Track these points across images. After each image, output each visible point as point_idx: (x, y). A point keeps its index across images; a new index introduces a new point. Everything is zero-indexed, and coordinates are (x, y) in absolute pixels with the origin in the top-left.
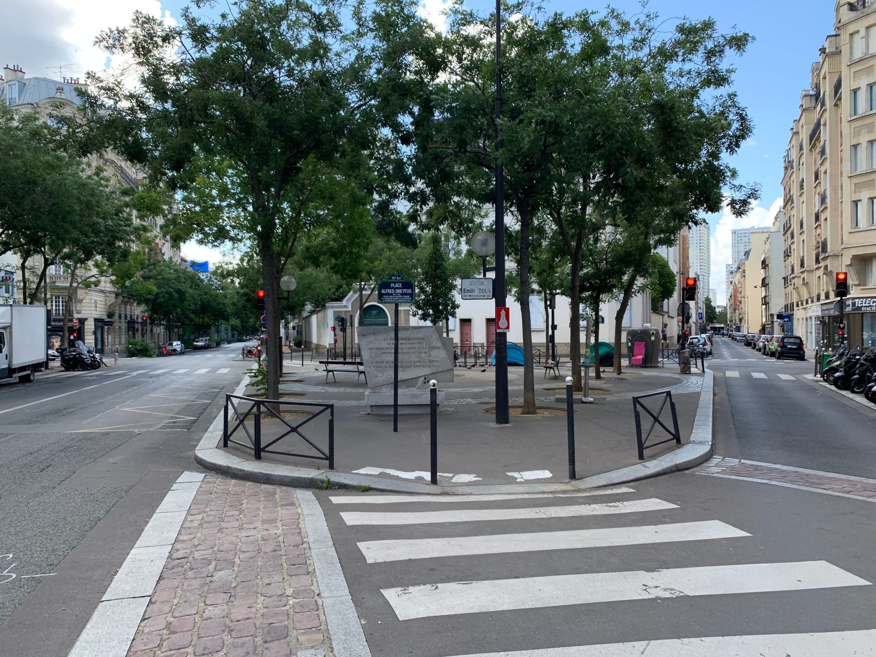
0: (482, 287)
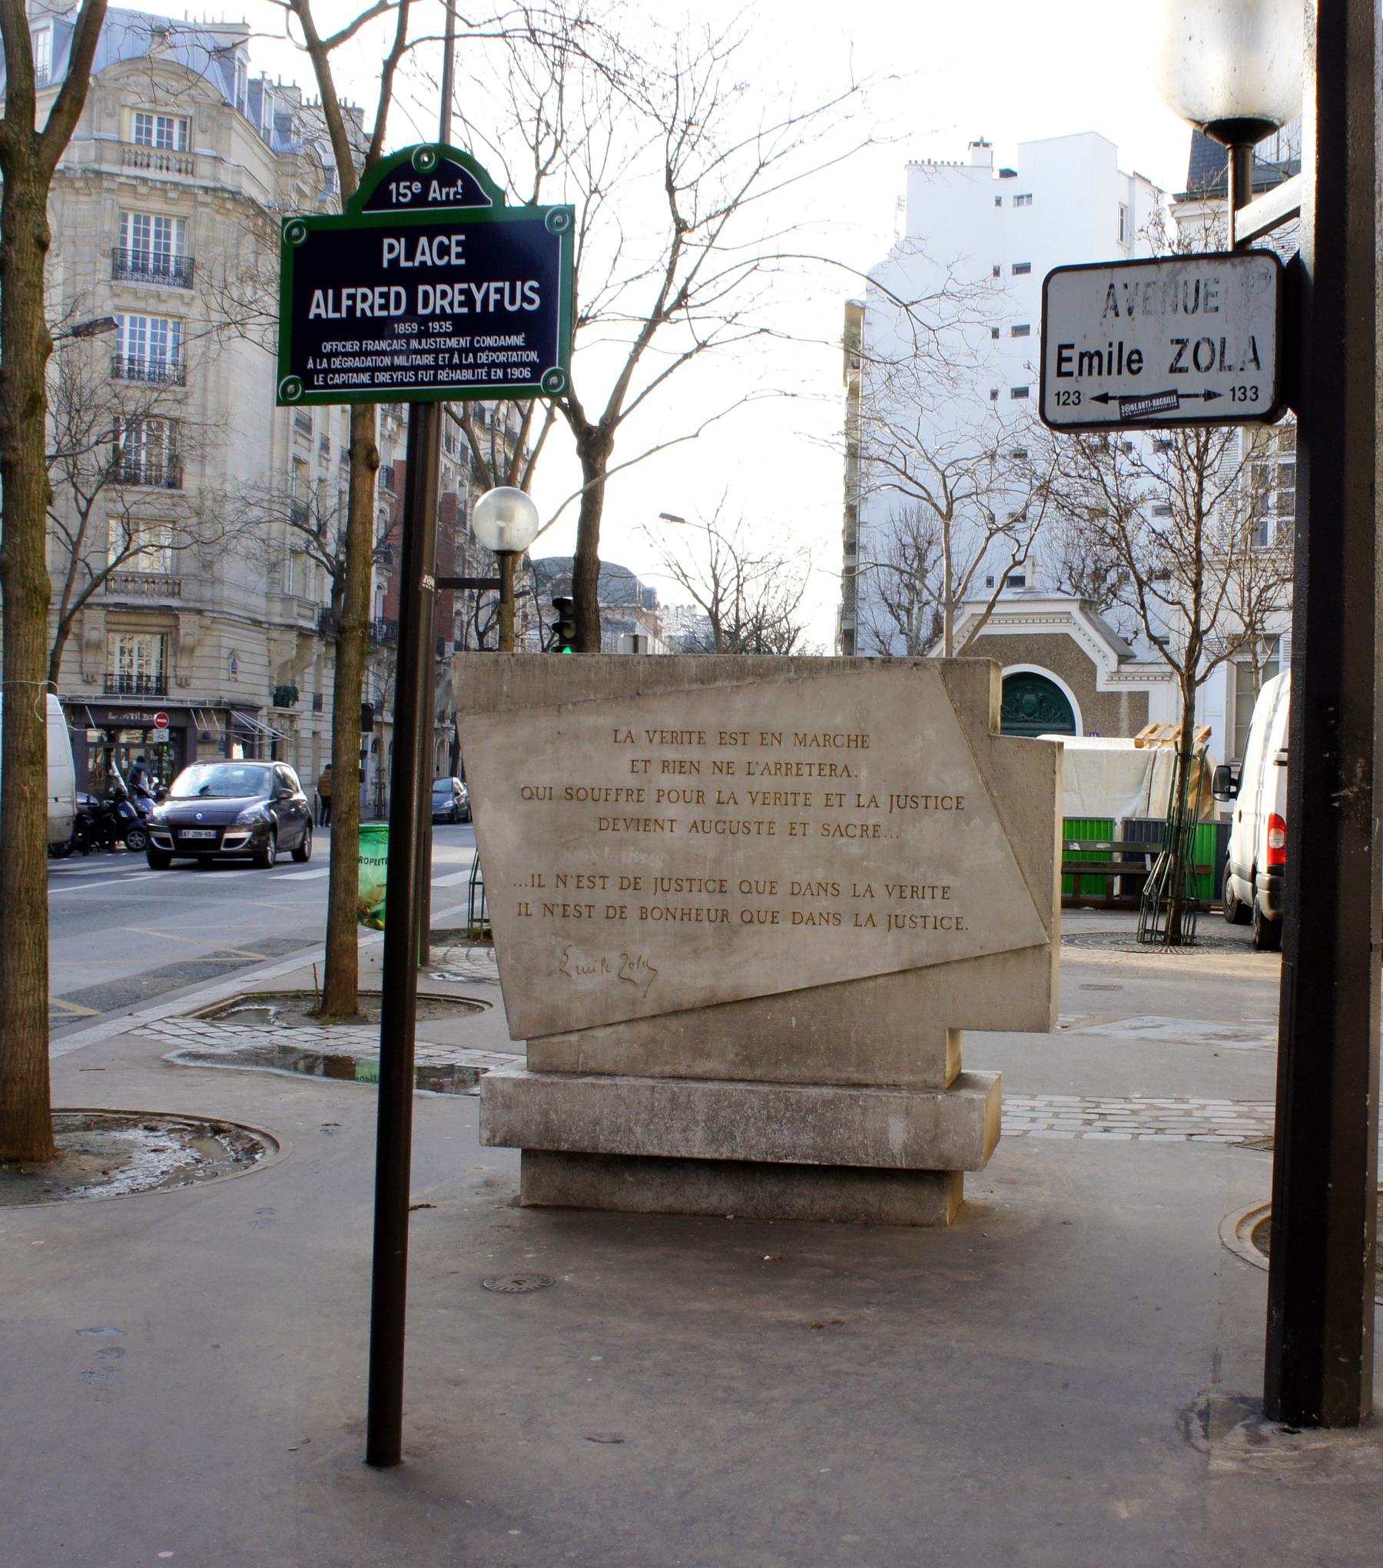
0: (1193, 327)
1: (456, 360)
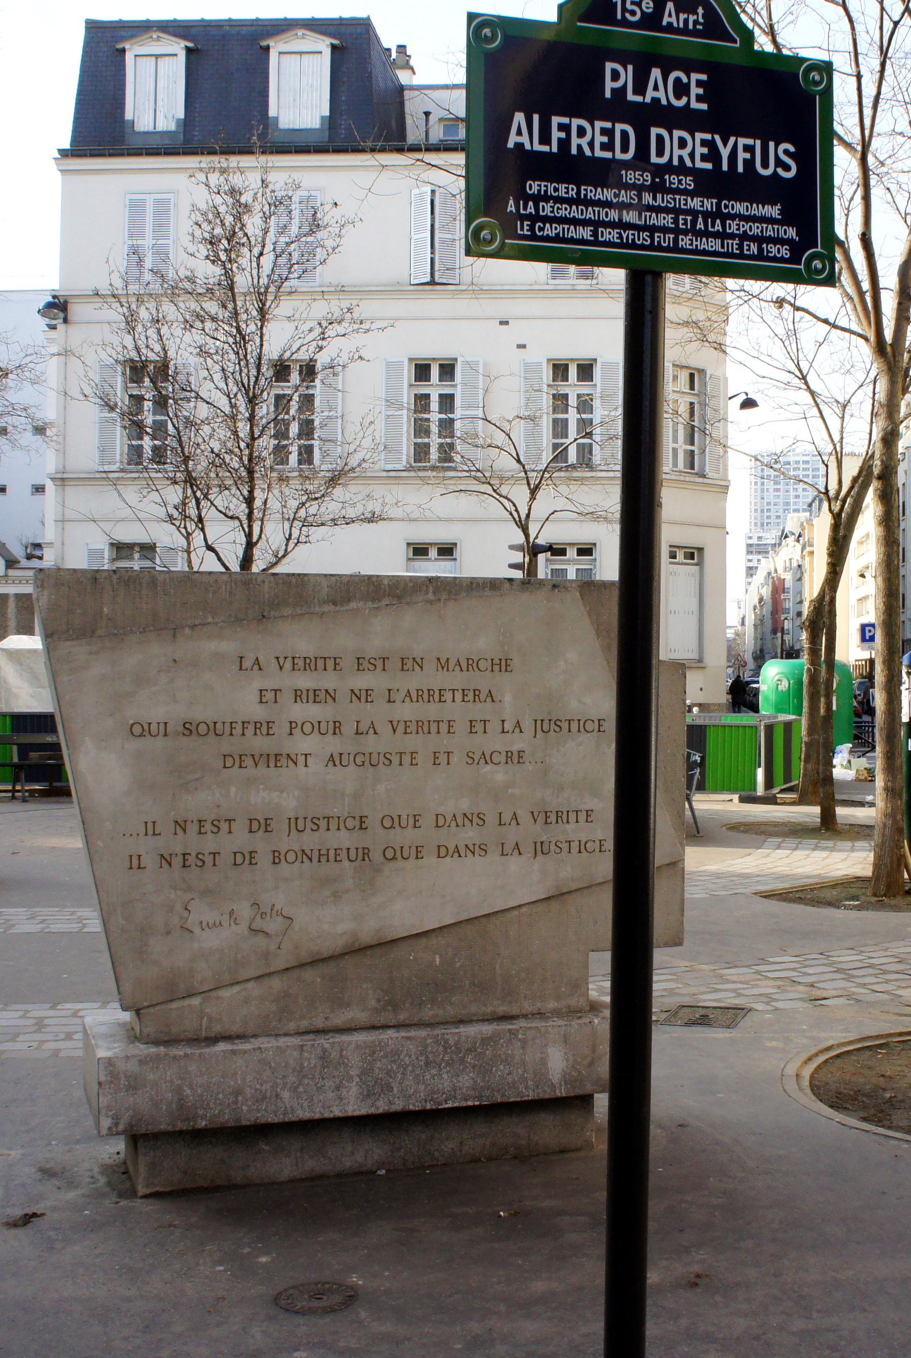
1: (700, 225)
